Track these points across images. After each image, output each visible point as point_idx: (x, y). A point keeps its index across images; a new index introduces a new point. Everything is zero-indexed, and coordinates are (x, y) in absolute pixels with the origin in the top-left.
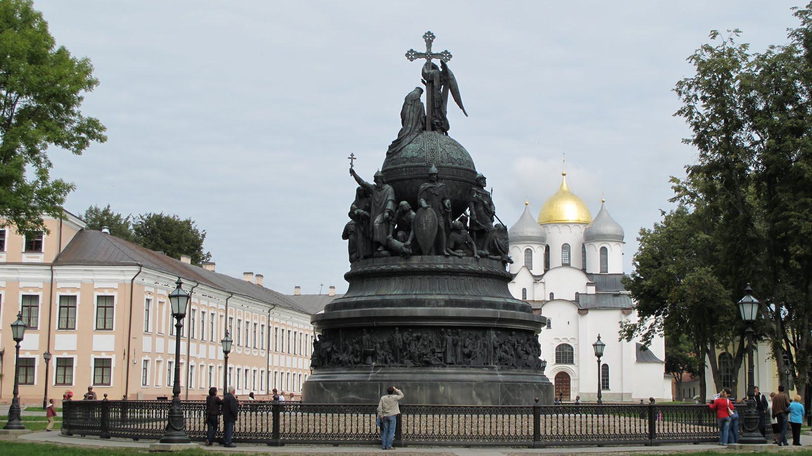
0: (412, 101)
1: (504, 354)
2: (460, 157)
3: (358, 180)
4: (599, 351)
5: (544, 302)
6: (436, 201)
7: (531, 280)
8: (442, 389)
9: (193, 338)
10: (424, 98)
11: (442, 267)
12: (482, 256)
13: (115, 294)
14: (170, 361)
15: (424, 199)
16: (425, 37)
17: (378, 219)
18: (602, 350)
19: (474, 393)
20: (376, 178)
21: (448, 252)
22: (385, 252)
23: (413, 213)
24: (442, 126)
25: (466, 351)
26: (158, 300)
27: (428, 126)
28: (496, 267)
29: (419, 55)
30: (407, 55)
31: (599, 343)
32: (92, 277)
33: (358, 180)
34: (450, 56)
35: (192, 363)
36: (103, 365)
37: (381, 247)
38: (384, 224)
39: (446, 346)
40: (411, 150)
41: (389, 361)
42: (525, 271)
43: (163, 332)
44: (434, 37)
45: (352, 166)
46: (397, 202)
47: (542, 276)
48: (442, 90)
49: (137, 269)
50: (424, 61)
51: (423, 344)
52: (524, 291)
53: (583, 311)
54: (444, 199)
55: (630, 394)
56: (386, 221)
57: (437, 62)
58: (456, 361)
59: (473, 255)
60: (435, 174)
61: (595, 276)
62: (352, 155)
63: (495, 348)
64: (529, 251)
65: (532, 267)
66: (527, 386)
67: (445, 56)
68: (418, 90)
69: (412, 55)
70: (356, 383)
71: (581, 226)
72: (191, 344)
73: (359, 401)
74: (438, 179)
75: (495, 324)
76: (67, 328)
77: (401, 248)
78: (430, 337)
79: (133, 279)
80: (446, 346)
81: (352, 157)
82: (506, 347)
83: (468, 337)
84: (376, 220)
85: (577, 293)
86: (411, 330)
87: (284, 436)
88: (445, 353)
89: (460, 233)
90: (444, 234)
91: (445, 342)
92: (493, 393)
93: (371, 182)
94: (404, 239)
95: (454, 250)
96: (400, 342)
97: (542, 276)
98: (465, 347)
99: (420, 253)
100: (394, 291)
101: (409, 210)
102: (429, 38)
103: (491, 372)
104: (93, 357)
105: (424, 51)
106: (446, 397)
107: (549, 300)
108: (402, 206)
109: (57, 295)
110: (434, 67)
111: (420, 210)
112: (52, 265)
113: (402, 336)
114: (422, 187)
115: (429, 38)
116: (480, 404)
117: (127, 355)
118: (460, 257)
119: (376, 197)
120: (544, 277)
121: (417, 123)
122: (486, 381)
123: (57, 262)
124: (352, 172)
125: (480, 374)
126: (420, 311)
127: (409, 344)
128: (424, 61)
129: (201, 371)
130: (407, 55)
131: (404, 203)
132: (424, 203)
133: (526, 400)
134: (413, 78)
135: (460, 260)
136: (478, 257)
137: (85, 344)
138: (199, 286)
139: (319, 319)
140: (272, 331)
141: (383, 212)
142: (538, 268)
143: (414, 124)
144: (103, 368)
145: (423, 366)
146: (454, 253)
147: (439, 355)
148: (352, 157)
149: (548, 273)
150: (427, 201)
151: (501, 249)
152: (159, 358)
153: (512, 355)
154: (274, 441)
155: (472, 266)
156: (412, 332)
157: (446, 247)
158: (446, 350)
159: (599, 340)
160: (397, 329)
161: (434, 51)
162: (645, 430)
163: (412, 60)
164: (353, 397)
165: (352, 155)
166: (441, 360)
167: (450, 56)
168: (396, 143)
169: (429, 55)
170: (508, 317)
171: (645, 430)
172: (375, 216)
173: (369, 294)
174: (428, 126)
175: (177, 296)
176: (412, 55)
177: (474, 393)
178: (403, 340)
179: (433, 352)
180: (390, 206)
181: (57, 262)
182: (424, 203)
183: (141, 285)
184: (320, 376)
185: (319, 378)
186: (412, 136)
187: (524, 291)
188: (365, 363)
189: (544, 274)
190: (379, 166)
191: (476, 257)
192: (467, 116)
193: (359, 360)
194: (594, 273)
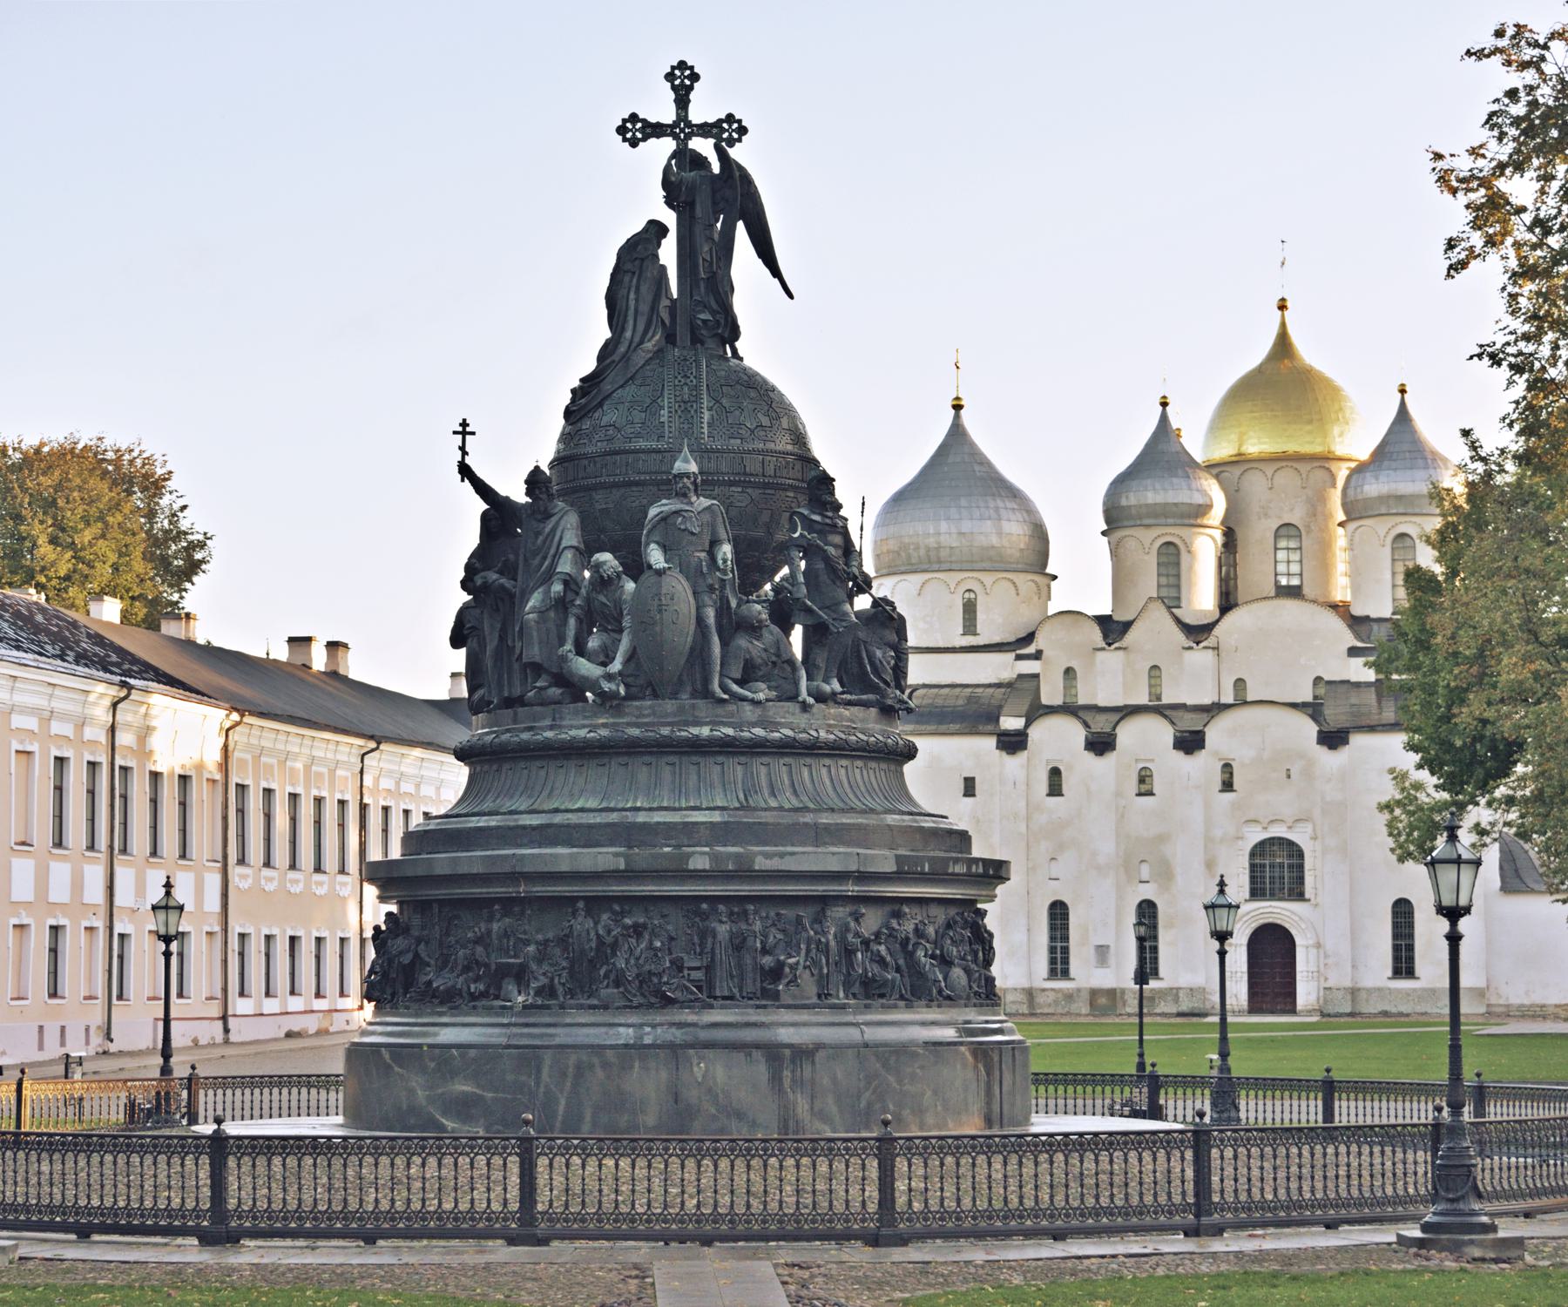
0: (637, 253)
1: (876, 968)
3: (482, 489)
4: (1222, 926)
5: (1216, 709)
7: (1180, 638)
8: (699, 1069)
9: (124, 851)
10: (668, 254)
11: (705, 731)
12: (821, 698)
14: (54, 923)
15: (657, 543)
16: (670, 77)
17: (534, 601)
20: (535, 481)
21: (725, 689)
22: (555, 692)
23: (630, 586)
25: (767, 961)
27: (682, 333)
29: (655, 130)
30: (621, 130)
31: (1221, 901)
33: (482, 489)
34: (743, 131)
37: (544, 676)
38: (552, 614)
39: (713, 949)
41: (560, 990)
42: (1159, 615)
44: (695, 77)
45: (465, 453)
46: (585, 553)
47: (1207, 628)
48: (719, 225)
50: (667, 145)
51: (650, 947)
53: (1333, 739)
54: (714, 543)
57: (703, 146)
58: (741, 991)
59: (793, 697)
61: (1375, 627)
62: (464, 424)
64: (1171, 549)
65: (1179, 599)
67: (728, 130)
68: (653, 230)
69: (635, 130)
70: (472, 1053)
75: (852, 889)
77: (597, 680)
78: (670, 927)
80: (713, 949)
81: (464, 430)
82: (882, 948)
83: (774, 925)
84: (530, 604)
85: (1318, 680)
86: (617, 908)
87: (240, 1218)
88: (709, 969)
90: (716, 639)
91: (710, 940)
92: (839, 1075)
93: (519, 495)
94: (607, 656)
95: (741, 683)
96: (590, 940)
97: (1207, 628)
98: (765, 951)
100: (581, 798)
101: (619, 577)
102: (683, 80)
103: (837, 1019)
105: (667, 115)
106: (710, 1090)
107: (1231, 701)
110: (699, 161)
111: (646, 577)
113: (596, 923)
114: (653, 512)
115: (683, 80)
120: (1217, 631)
124: (465, 471)
125: (805, 1024)
127: (615, 946)
128: (667, 145)
130: (621, 130)
131: (606, 557)
132: (656, 557)
133: (935, 1092)
134: (637, 192)
135: (759, 711)
136: (811, 700)
139: (382, 874)
140: (374, 819)
141: (548, 578)
142: (1202, 597)
143: (641, 327)
145: (651, 1006)
146: (740, 691)
148: (464, 430)
149: (1231, 617)
150: (665, 548)
153: (898, 970)
156: (623, 914)
157: (722, 675)
158: (713, 960)
159: (1222, 892)
160: (581, 904)
161: (697, 115)
162: (1184, 1193)
163: (634, 143)
164: (465, 1088)
165: (464, 424)
166: (699, 988)
167: (743, 131)
169: (682, 128)
171: (1184, 1193)
172: (525, 595)
173: (522, 807)
176: (635, 130)
178: (598, 935)
179: (678, 966)
182: (656, 557)
185: (381, 1034)
188: (497, 997)
189: (1217, 621)
190: (544, 453)
191: (804, 702)
192: (791, 296)
193: (482, 987)
194: (1373, 615)
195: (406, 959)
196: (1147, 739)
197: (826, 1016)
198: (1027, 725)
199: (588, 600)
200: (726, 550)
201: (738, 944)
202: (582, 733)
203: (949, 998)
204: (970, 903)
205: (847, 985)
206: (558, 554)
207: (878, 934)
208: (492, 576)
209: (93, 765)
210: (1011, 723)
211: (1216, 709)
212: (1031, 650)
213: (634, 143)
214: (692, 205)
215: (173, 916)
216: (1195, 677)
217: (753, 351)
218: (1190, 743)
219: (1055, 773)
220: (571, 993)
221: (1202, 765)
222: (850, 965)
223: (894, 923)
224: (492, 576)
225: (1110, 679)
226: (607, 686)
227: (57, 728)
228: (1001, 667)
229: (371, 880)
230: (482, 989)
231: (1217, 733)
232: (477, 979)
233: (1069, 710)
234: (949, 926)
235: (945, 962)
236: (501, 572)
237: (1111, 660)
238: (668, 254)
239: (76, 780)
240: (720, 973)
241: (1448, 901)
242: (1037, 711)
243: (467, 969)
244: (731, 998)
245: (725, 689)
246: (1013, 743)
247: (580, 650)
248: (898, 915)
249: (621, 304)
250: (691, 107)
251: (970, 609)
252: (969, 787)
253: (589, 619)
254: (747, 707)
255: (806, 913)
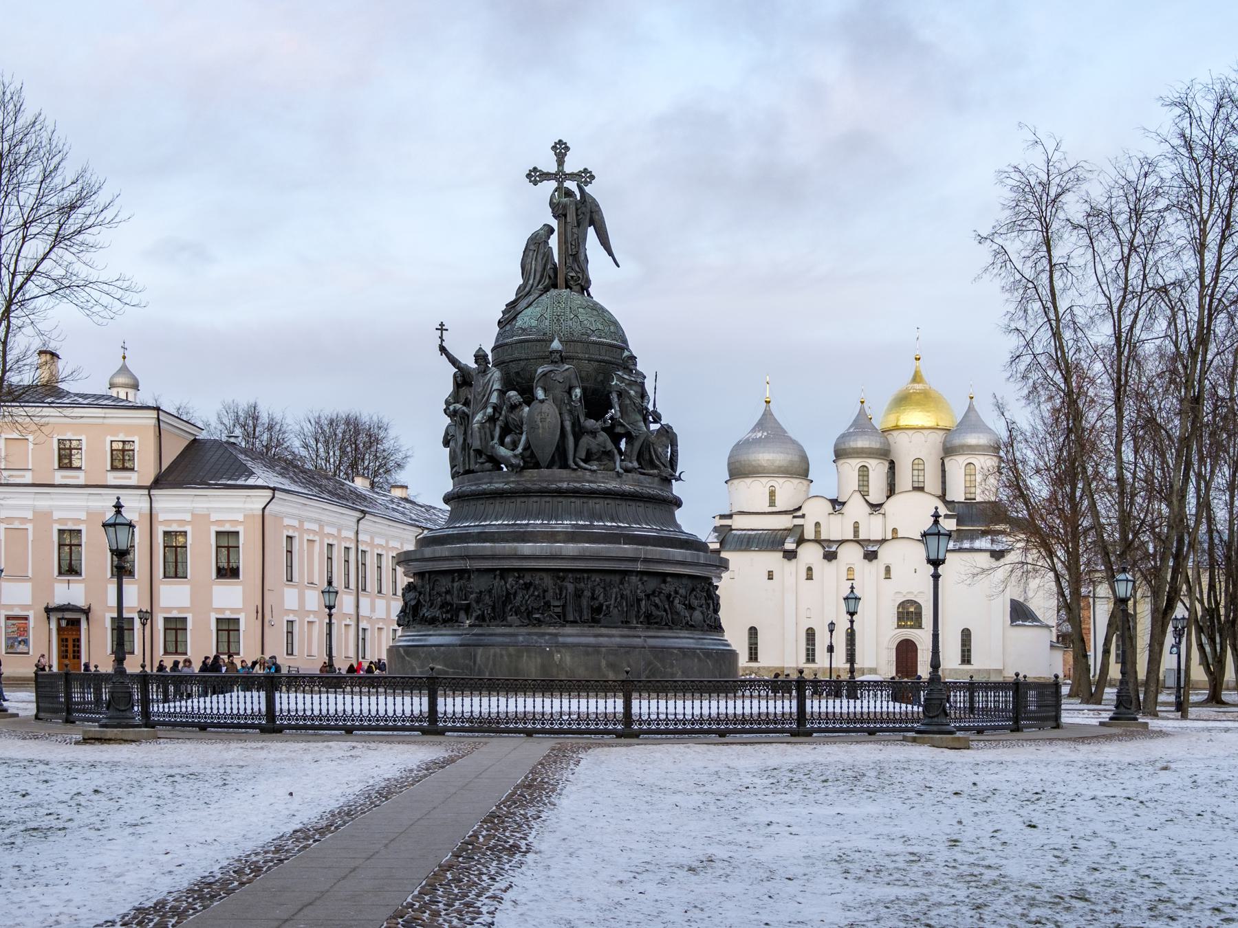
0: (537, 243)
2: (600, 327)
3: (453, 361)
5: (884, 541)
6: (559, 392)
7: (868, 509)
9: (364, 590)
10: (553, 242)
11: (565, 485)
12: (627, 470)
13: (240, 529)
16: (554, 148)
17: (478, 417)
18: (856, 606)
19: (603, 663)
20: (480, 357)
21: (576, 464)
24: (583, 286)
25: (596, 604)
26: (306, 537)
28: (650, 486)
29: (546, 176)
30: (529, 176)
32: (51, 503)
33: (453, 361)
34: (592, 177)
35: (363, 625)
36: (228, 627)
40: (527, 318)
42: (858, 496)
43: (316, 581)
44: (567, 149)
45: (442, 340)
46: (502, 393)
47: (880, 505)
49: (269, 493)
50: (553, 184)
52: (817, 524)
55: (1000, 671)
56: (492, 419)
57: (571, 185)
60: (557, 351)
62: (442, 325)
63: (639, 601)
66: (685, 654)
67: (585, 177)
69: (536, 176)
71: (941, 433)
72: (361, 599)
73: (446, 673)
74: (563, 359)
75: (640, 567)
76: (176, 576)
79: (264, 508)
88: (564, 606)
89: (595, 437)
90: (571, 440)
93: (472, 365)
95: (585, 461)
97: (880, 505)
99: (537, 466)
102: (561, 150)
104: (213, 616)
105: (553, 168)
108: (509, 398)
109: (159, 530)
110: (569, 193)
112: (150, 488)
114: (540, 371)
115: (561, 150)
116: (611, 676)
117: (261, 613)
118: (594, 471)
119: (479, 382)
121: (542, 276)
122: (620, 646)
123: (160, 482)
124: (443, 349)
126: (527, 548)
128: (553, 184)
129: (310, 631)
130: (529, 176)
131: (512, 393)
137: (201, 597)
138: (368, 517)
141: (485, 407)
142: (876, 495)
144: (229, 631)
147: (558, 610)
148: (442, 328)
149: (892, 499)
150: (545, 390)
151: (658, 458)
152: (311, 618)
153: (665, 610)
154: (271, 725)
155: (613, 485)
156: (519, 577)
161: (569, 168)
163: (535, 183)
165: (442, 325)
167: (592, 177)
168: (512, 306)
169: (560, 176)
170: (507, 552)
172: (474, 414)
174: (561, 281)
175: (114, 525)
176: (536, 176)
177: (603, 663)
180: (494, 399)
181: (160, 482)
182: (540, 394)
183: (278, 518)
184: (404, 637)
186: (531, 298)
187: (817, 524)
195: (413, 603)
196: (851, 555)
197: (626, 632)
198: (798, 546)
199: (506, 417)
200: (578, 391)
201: (578, 594)
202: (501, 486)
203: (692, 626)
204: (707, 580)
205: (638, 617)
206: (491, 393)
207: (654, 592)
208: (459, 406)
209: (347, 549)
210: (790, 545)
211: (884, 541)
212: (799, 513)
213: (535, 183)
214: (565, 216)
215: (332, 596)
216: (873, 528)
217: (597, 292)
218: (871, 556)
219: (810, 569)
220: (494, 618)
221: (878, 566)
222: (639, 606)
223: (663, 586)
224: (459, 406)
225: (836, 528)
226: (514, 461)
227: (327, 530)
228: (785, 522)
229: (398, 563)
230: (450, 616)
231: (885, 553)
232: (447, 612)
233: (817, 541)
234: (693, 590)
235: (691, 608)
236: (464, 404)
237: (836, 519)
238: (553, 242)
239: (338, 555)
240: (570, 609)
241: (932, 557)
242: (801, 541)
243: (442, 607)
244: (574, 622)
245: (576, 464)
246: (790, 555)
247: (502, 444)
248: (665, 582)
249: (528, 267)
250: (566, 165)
251: (772, 494)
252: (770, 576)
253: (506, 431)
254: (588, 473)
255: (617, 578)
